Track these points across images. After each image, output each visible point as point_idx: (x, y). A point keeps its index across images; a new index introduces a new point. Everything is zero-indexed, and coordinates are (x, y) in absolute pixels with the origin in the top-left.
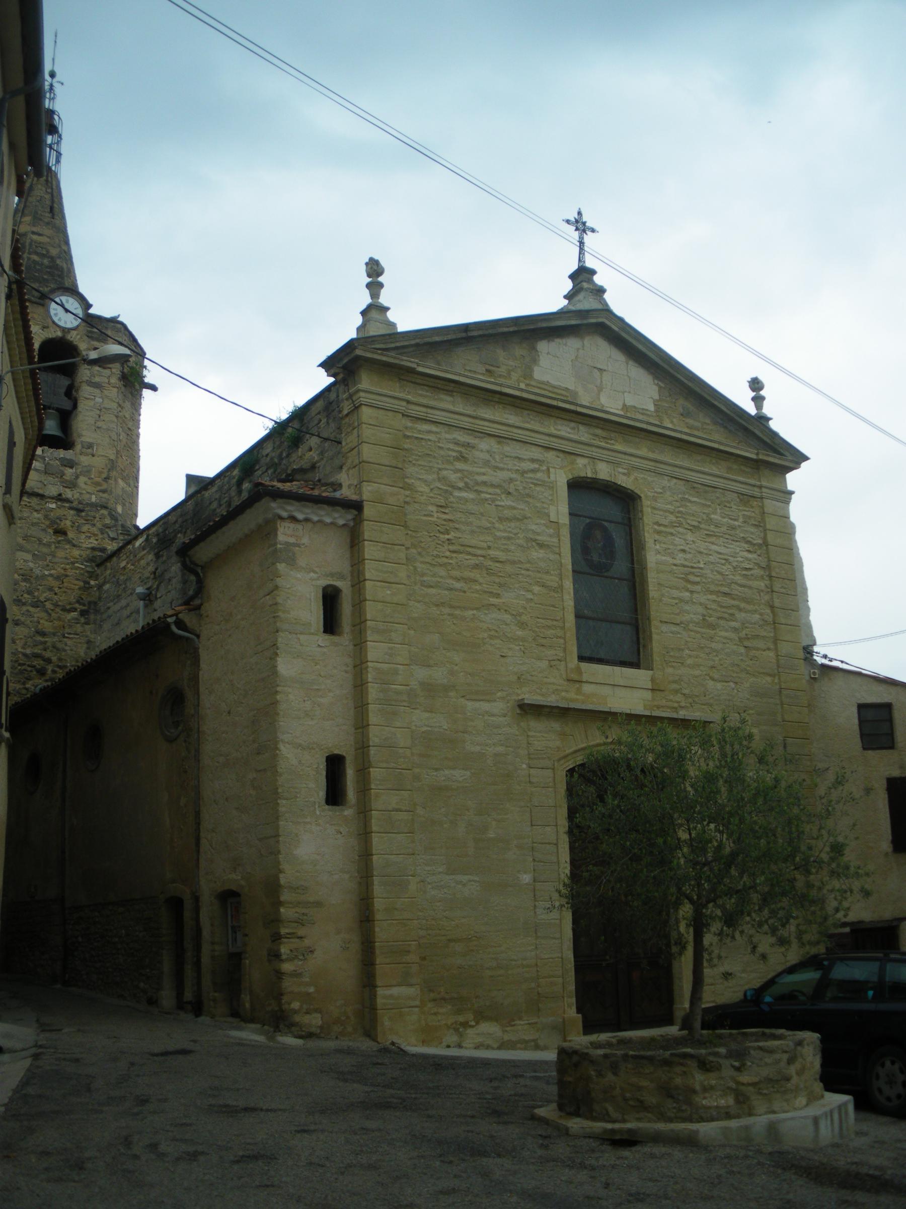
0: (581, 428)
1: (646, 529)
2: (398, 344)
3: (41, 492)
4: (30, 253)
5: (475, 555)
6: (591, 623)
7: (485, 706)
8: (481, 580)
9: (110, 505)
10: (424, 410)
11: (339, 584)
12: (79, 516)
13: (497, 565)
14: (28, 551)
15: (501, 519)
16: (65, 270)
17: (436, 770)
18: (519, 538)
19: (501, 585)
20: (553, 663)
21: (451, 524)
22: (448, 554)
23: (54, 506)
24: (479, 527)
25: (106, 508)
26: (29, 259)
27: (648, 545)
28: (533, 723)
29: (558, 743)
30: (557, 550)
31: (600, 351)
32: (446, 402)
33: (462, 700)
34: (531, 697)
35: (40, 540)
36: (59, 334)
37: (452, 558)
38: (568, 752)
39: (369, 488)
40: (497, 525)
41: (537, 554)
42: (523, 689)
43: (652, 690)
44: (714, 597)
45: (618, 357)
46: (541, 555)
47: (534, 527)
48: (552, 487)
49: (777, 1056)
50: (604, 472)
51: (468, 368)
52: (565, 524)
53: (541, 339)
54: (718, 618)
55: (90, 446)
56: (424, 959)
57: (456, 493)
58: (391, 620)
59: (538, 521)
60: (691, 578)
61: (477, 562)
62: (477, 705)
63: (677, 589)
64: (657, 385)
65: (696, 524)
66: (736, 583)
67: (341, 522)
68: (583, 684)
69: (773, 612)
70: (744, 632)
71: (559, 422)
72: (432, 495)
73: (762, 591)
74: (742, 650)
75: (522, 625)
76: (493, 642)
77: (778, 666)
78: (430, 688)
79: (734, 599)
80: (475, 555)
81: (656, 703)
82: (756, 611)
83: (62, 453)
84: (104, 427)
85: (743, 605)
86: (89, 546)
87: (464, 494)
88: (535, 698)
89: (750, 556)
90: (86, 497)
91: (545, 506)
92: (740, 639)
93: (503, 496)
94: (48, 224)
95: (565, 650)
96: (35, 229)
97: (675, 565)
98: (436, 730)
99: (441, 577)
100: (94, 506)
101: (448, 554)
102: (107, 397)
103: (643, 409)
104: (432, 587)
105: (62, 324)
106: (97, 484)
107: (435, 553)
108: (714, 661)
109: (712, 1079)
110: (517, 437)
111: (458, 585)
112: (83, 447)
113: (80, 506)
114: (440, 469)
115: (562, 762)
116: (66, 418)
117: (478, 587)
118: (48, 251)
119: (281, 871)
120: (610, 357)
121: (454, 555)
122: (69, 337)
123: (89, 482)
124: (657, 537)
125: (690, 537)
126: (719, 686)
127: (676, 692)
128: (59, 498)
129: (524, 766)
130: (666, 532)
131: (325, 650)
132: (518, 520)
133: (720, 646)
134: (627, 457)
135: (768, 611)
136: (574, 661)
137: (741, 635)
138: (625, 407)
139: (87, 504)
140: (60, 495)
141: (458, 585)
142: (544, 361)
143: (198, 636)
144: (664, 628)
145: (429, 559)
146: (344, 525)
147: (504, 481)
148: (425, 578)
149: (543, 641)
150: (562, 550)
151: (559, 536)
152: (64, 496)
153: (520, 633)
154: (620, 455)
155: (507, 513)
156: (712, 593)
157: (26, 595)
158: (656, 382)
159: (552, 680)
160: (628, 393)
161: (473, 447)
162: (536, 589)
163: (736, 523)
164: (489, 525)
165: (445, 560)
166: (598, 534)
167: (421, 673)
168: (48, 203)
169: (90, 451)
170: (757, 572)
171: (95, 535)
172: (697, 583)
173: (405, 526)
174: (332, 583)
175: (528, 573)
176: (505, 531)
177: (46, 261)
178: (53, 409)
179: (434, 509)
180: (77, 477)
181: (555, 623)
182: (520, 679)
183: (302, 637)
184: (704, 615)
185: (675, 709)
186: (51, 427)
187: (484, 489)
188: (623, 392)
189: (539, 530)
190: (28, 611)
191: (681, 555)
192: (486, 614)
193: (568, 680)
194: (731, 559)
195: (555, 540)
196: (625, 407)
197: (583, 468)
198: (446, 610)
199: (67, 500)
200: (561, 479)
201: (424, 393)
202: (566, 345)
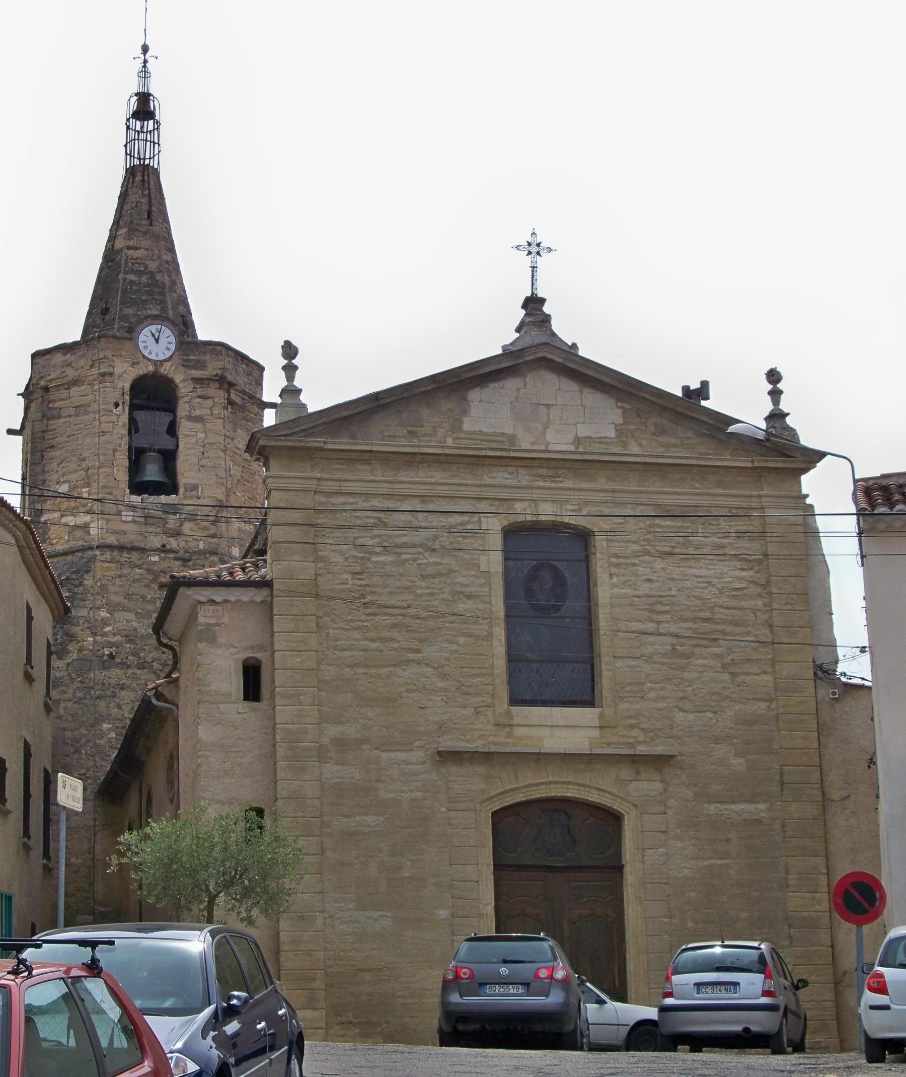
0: (521, 470)
1: (599, 563)
2: (303, 428)
3: (142, 545)
4: (126, 273)
7: (401, 756)
8: (399, 638)
9: (220, 551)
10: (338, 484)
11: (258, 655)
12: (185, 566)
13: (418, 621)
14: (130, 611)
15: (423, 577)
16: (168, 285)
17: (347, 816)
18: (444, 593)
19: (420, 641)
20: (478, 710)
21: (368, 589)
22: (363, 617)
23: (156, 559)
24: (398, 588)
25: (216, 554)
26: (125, 280)
27: (599, 581)
28: (453, 769)
29: (483, 786)
30: (487, 599)
31: (547, 386)
32: (364, 472)
34: (449, 743)
35: (143, 598)
36: (151, 368)
37: (367, 621)
39: (279, 567)
40: (418, 583)
42: (445, 737)
43: (601, 727)
44: (690, 624)
45: (570, 386)
46: (468, 606)
47: (461, 580)
50: (547, 512)
51: (386, 434)
53: (472, 388)
54: (694, 646)
55: (194, 487)
58: (300, 685)
60: (658, 608)
61: (395, 621)
62: (392, 755)
63: (638, 621)
64: (622, 407)
66: (721, 606)
67: (259, 599)
68: (515, 728)
70: (730, 658)
71: (495, 469)
72: (346, 563)
73: (759, 610)
74: (727, 677)
75: (445, 677)
76: (411, 695)
78: (341, 744)
79: (717, 623)
81: (605, 740)
83: (163, 499)
85: (729, 629)
87: (383, 558)
88: (458, 744)
89: (744, 574)
91: (475, 557)
92: (724, 666)
93: (427, 555)
94: (146, 233)
95: (493, 696)
96: (131, 243)
98: (347, 780)
99: (356, 640)
100: (203, 553)
101: (363, 617)
103: (600, 438)
104: (346, 650)
105: (153, 357)
107: (350, 618)
108: (686, 692)
110: (443, 493)
111: (373, 645)
112: (186, 491)
114: (356, 538)
115: (486, 804)
116: (169, 458)
117: (395, 645)
118: (146, 267)
120: (559, 389)
122: (162, 370)
123: (195, 528)
124: (613, 570)
125: (659, 564)
126: (691, 717)
127: (633, 727)
128: (163, 549)
129: (444, 809)
130: (625, 564)
131: (245, 716)
132: (443, 575)
133: (696, 675)
134: (576, 493)
135: (768, 632)
136: (503, 704)
137: (725, 661)
138: (578, 441)
139: (195, 552)
140: (164, 546)
142: (476, 410)
143: (177, 706)
146: (262, 602)
147: (428, 539)
148: (338, 643)
149: (469, 690)
150: (493, 598)
151: (489, 585)
152: (168, 547)
153: (441, 684)
154: (567, 492)
155: (431, 570)
157: (130, 658)
158: (620, 404)
159: (478, 726)
160: (574, 423)
162: (462, 640)
164: (409, 584)
166: (547, 575)
167: (333, 730)
168: (145, 207)
169: (194, 493)
170: (753, 590)
172: (667, 612)
173: (317, 596)
174: (251, 655)
175: (453, 625)
176: (428, 588)
177: (144, 279)
178: (154, 451)
179: (349, 576)
180: (181, 525)
181: (483, 671)
182: (442, 728)
183: (221, 706)
184: (673, 645)
185: (632, 745)
186: (152, 472)
188: (575, 425)
190: (133, 673)
191: (646, 585)
192: (404, 670)
193: (497, 725)
194: (715, 581)
196: (578, 441)
197: (523, 512)
198: (361, 670)
199: (171, 551)
200: (494, 525)
201: (337, 466)
202: (503, 388)
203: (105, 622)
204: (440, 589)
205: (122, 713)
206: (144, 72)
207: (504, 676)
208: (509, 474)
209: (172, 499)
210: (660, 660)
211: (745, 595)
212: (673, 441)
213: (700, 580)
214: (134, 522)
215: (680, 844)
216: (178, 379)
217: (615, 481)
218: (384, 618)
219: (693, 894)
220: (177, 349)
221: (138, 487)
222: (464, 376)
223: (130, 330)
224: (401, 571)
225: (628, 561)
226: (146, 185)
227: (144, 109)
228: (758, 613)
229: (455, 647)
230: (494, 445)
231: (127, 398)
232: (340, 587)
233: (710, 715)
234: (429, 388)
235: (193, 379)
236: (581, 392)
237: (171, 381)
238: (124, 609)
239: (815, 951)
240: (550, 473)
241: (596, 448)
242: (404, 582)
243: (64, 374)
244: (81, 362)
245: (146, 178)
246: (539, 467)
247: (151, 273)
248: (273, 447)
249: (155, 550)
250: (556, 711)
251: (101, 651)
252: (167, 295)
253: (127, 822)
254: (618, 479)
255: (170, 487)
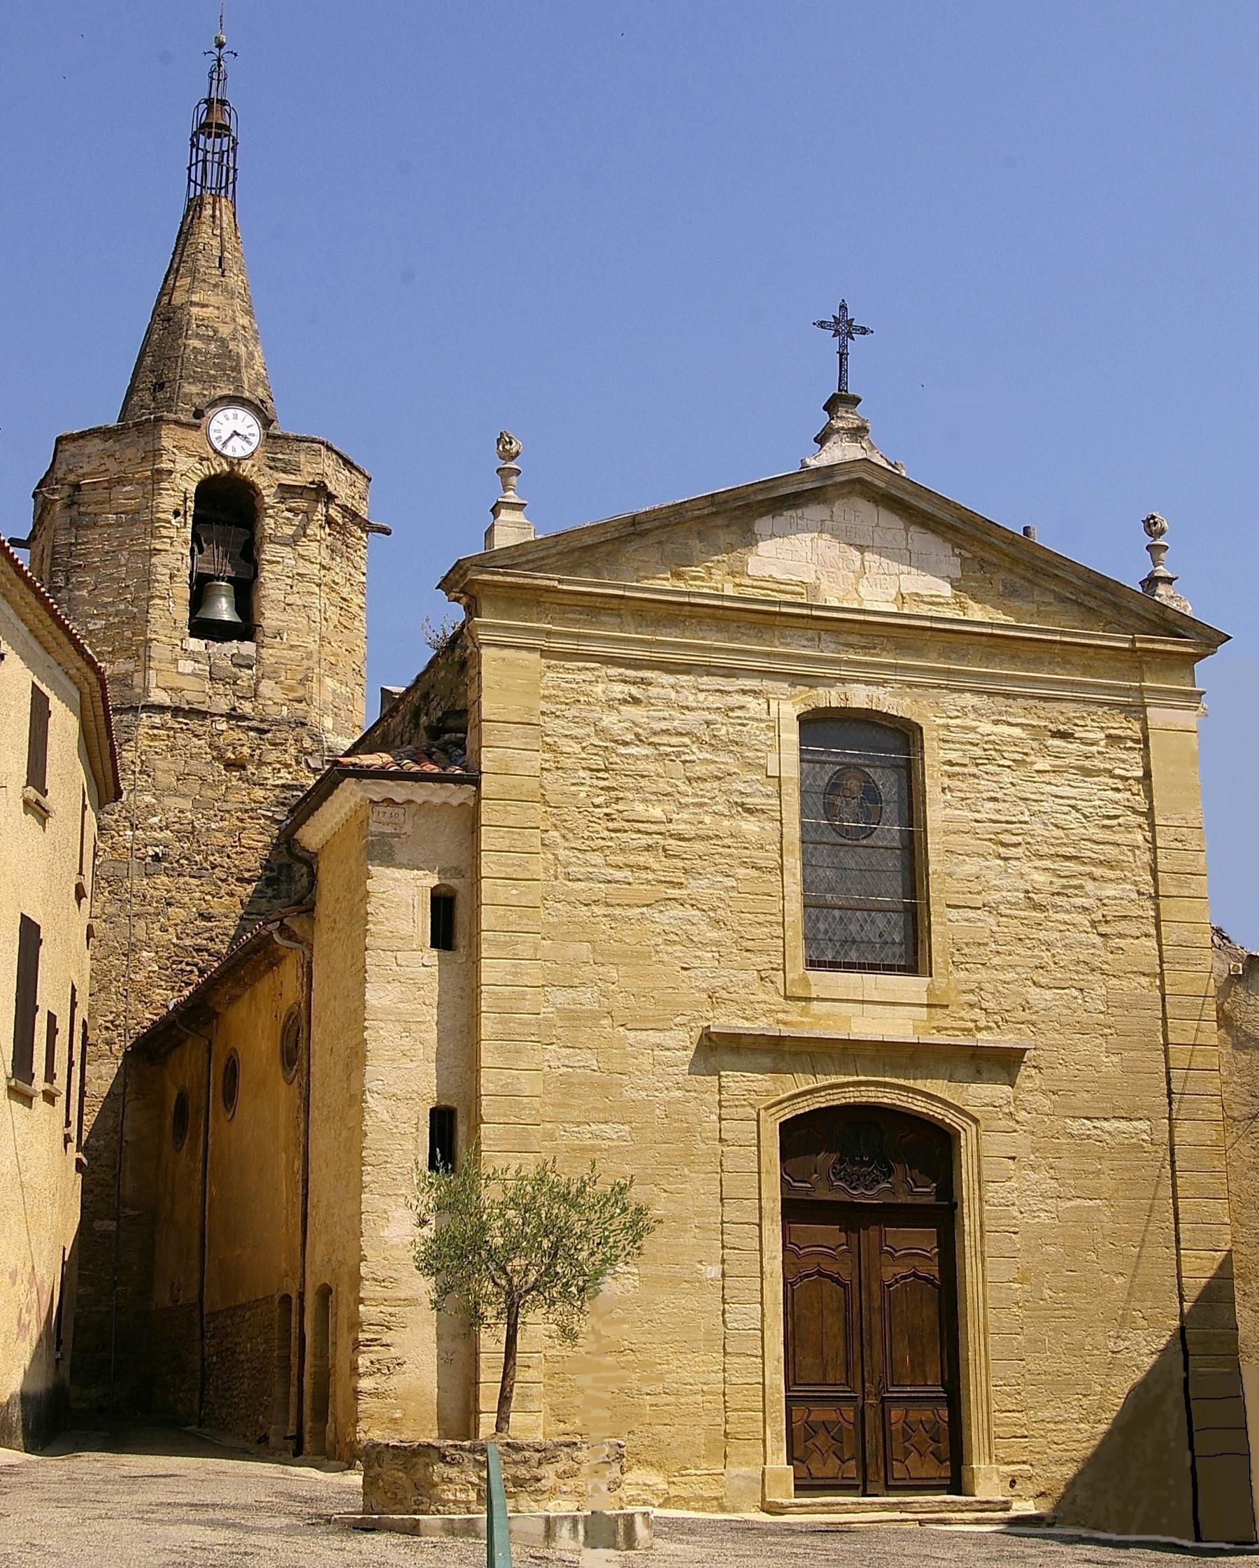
2: (530, 557)
5: (648, 833)
6: (837, 913)
7: (653, 1037)
8: (655, 866)
11: (453, 882)
14: (184, 796)
17: (578, 1124)
18: (717, 803)
23: (224, 726)
33: (621, 1029)
34: (727, 1021)
35: (203, 780)
38: (783, 1096)
41: (750, 826)
48: (775, 726)
49: (527, 1454)
50: (860, 697)
52: (792, 778)
53: (761, 516)
56: (552, 1376)
57: (623, 750)
59: (748, 778)
60: (1006, 838)
61: (650, 842)
65: (1018, 757)
69: (1155, 878)
74: (1098, 940)
77: (1162, 962)
78: (572, 1017)
80: (648, 833)
82: (1125, 879)
84: (300, 602)
85: (1098, 871)
86: (279, 782)
89: (1118, 796)
90: (272, 710)
92: (1093, 924)
94: (216, 286)
97: (976, 821)
101: (606, 834)
102: (302, 557)
106: (291, 689)
107: (586, 834)
109: (452, 1472)
111: (619, 875)
113: (264, 726)
115: (773, 1110)
117: (651, 876)
119: (364, 1258)
121: (613, 835)
126: (1048, 994)
128: (233, 716)
136: (797, 967)
140: (234, 709)
141: (619, 875)
144: (953, 914)
145: (578, 844)
149: (750, 944)
153: (714, 935)
155: (700, 770)
156: (1041, 857)
158: (957, 551)
161: (650, 684)
162: (741, 872)
163: (1094, 749)
164: (670, 790)
165: (602, 843)
167: (560, 997)
168: (216, 252)
171: (287, 766)
177: (212, 347)
181: (770, 918)
186: (224, 610)
187: (665, 739)
189: (749, 790)
195: (776, 801)
199: (244, 718)
202: (802, 518)
203: (151, 810)
204: (711, 799)
205: (167, 937)
206: (217, 73)
207: (800, 927)
208: (807, 640)
209: (248, 648)
210: (1009, 912)
211: (1119, 825)
212: (1028, 607)
213: (1061, 801)
214: (193, 674)
215: (1034, 1176)
216: (261, 482)
217: (950, 658)
218: (634, 836)
219: (1051, 1249)
220: (261, 444)
221: (203, 628)
222: (753, 498)
223: (199, 414)
224: (661, 771)
225: (966, 770)
226: (218, 222)
227: (212, 124)
228: (1137, 852)
229: (730, 882)
230: (788, 598)
231: (191, 504)
232: (573, 788)
233: (1075, 993)
234: (706, 512)
235: (280, 485)
236: (907, 531)
237: (252, 486)
238: (176, 793)
239: (1214, 1335)
240: (863, 642)
241: (924, 610)
242: (663, 786)
243: (103, 468)
244: (130, 453)
245: (218, 213)
246: (850, 633)
247: (222, 340)
248: (486, 583)
249: (222, 716)
250: (870, 978)
251: (143, 850)
252: (243, 370)
253: (174, 1094)
254: (953, 656)
255: (245, 628)
